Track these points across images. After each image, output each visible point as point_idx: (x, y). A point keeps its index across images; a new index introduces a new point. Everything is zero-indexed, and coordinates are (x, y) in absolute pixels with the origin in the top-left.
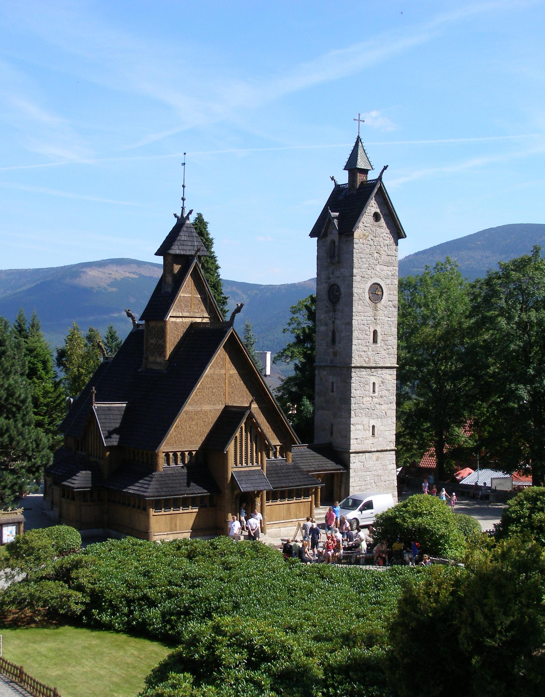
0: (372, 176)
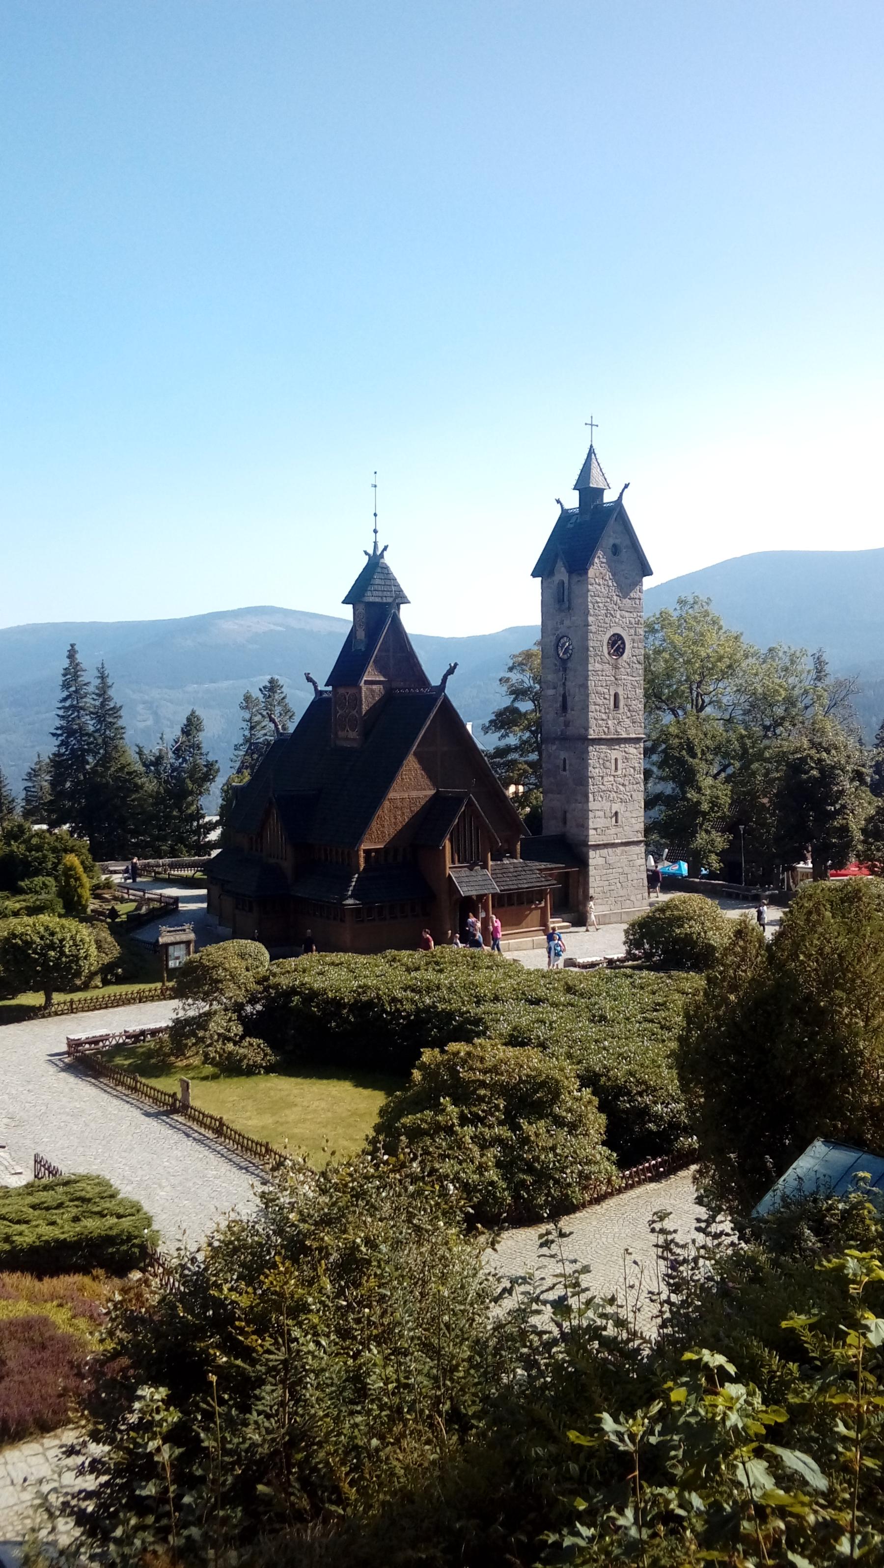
0: (609, 497)
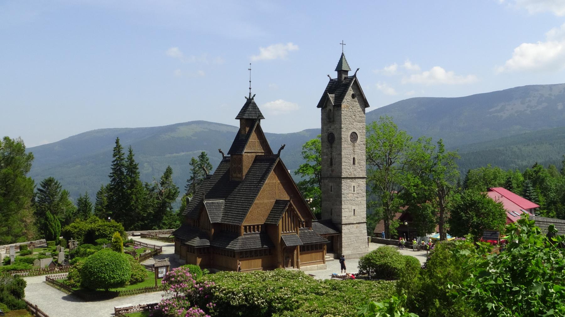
0: (350, 74)
